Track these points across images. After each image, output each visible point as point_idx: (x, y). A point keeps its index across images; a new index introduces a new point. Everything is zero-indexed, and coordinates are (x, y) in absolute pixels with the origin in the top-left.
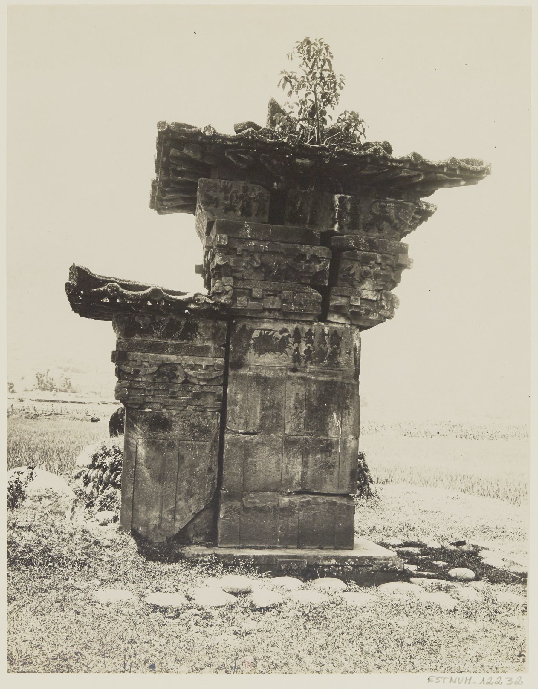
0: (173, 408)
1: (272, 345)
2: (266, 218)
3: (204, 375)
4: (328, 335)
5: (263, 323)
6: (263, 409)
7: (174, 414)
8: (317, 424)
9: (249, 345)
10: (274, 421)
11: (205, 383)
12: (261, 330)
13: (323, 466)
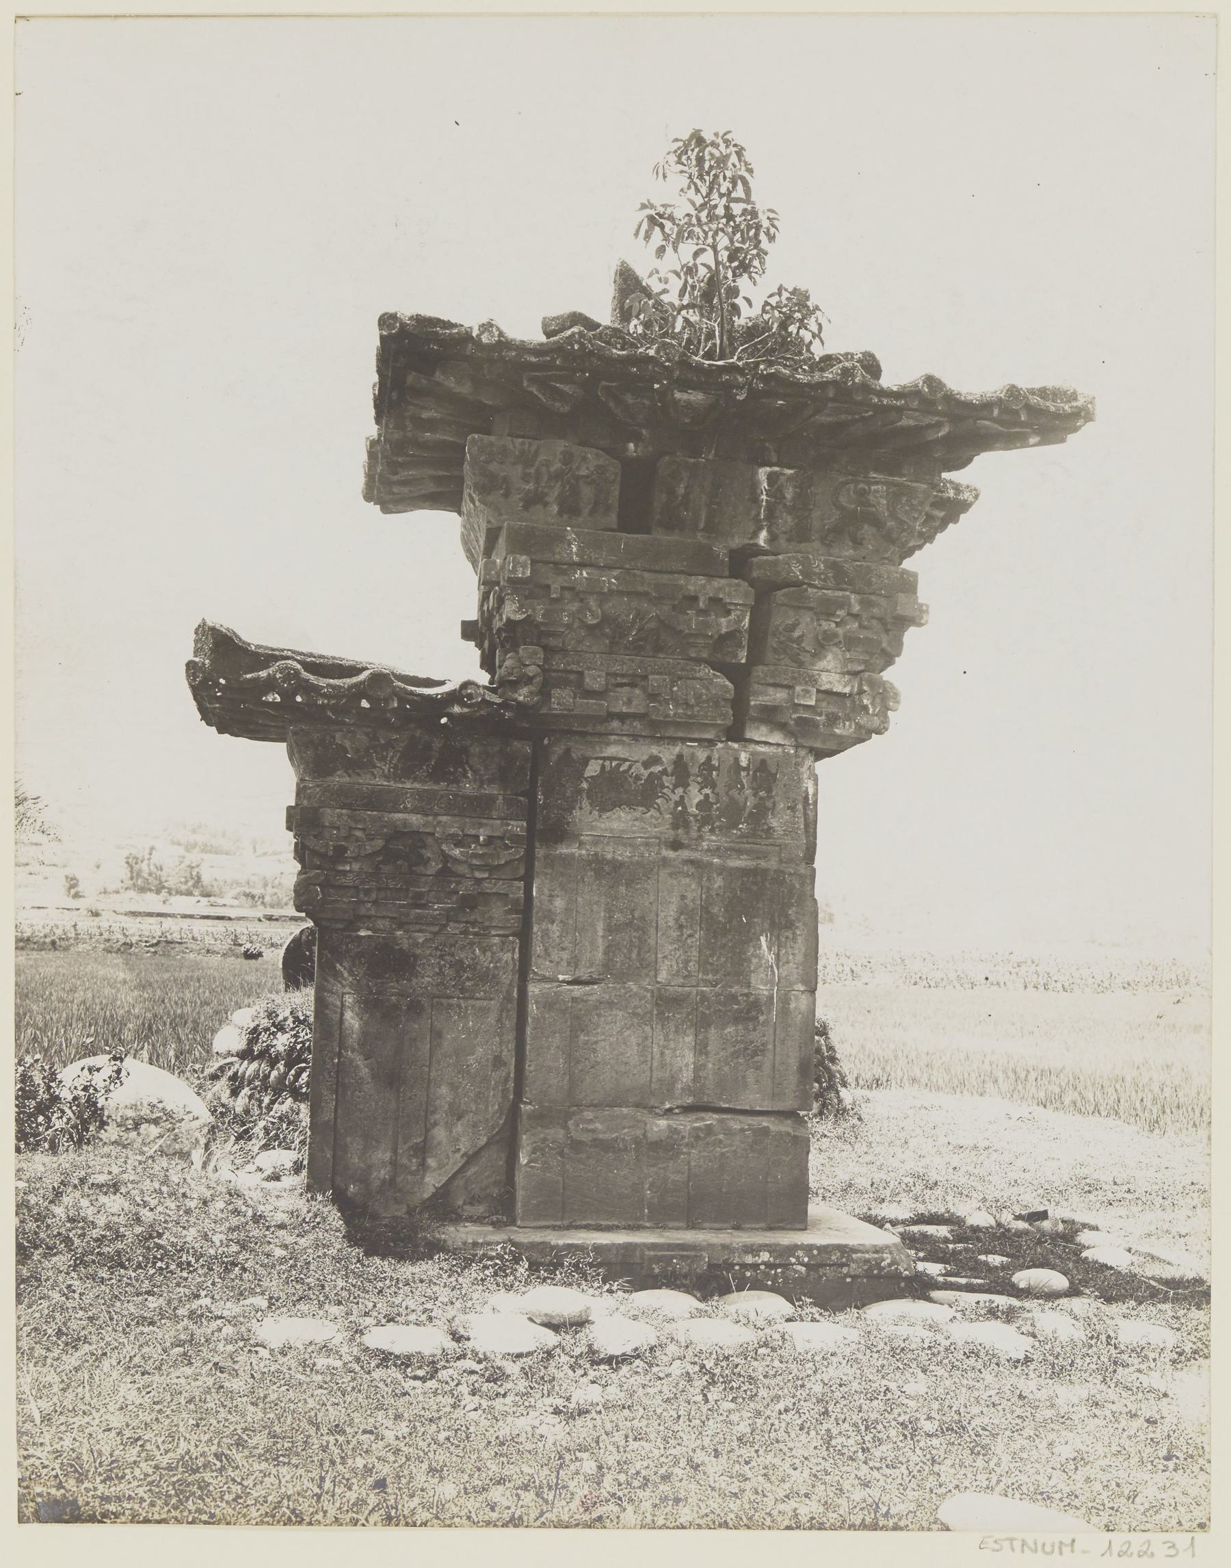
0: (418, 927)
2: (613, 519)
3: (482, 856)
4: (747, 769)
5: (608, 744)
6: (609, 930)
7: (420, 941)
9: (579, 791)
10: (634, 956)
11: (486, 875)
12: (604, 759)
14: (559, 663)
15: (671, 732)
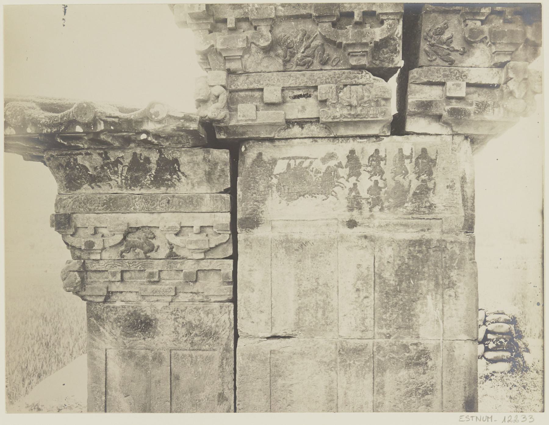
0: (155, 298)
1: (309, 183)
3: (196, 242)
4: (410, 157)
8: (397, 318)
9: (270, 187)
12: (289, 158)
13: (411, 391)
14: (241, 83)
15: (342, 131)
